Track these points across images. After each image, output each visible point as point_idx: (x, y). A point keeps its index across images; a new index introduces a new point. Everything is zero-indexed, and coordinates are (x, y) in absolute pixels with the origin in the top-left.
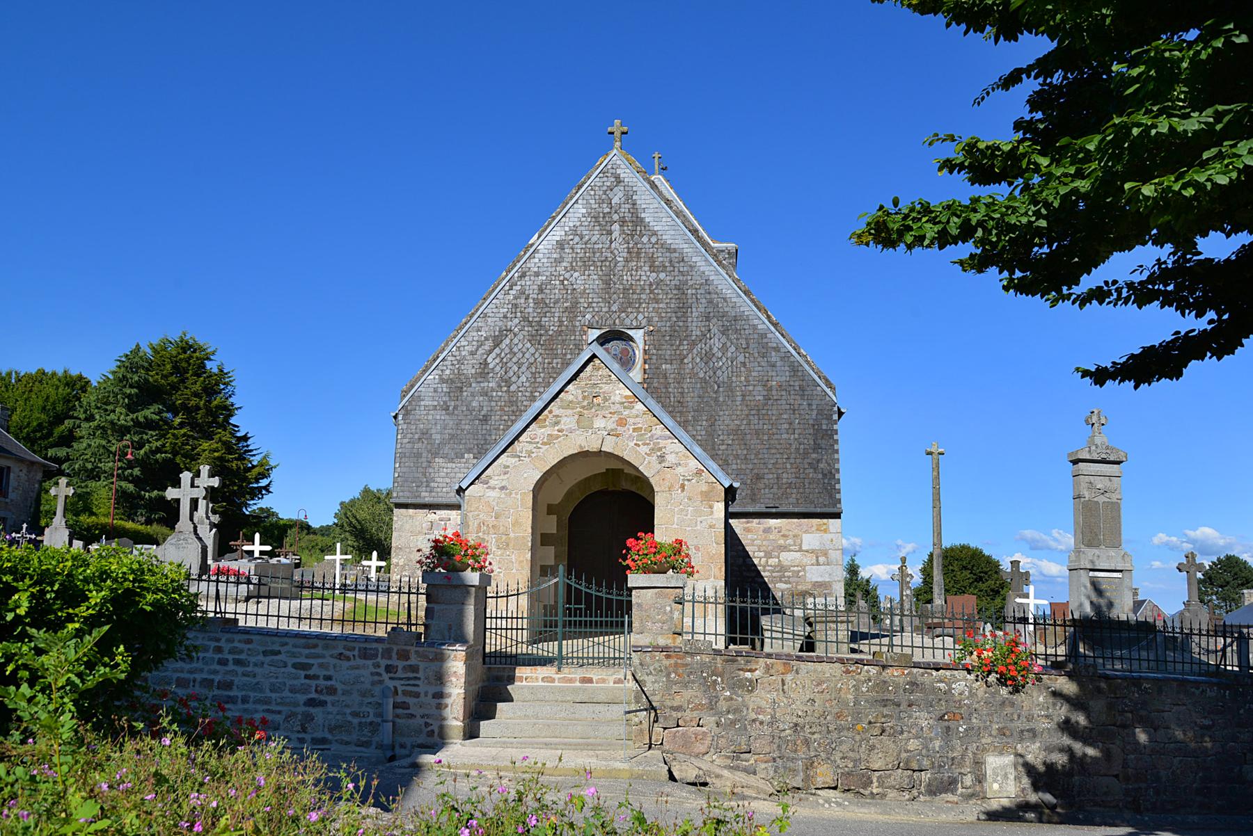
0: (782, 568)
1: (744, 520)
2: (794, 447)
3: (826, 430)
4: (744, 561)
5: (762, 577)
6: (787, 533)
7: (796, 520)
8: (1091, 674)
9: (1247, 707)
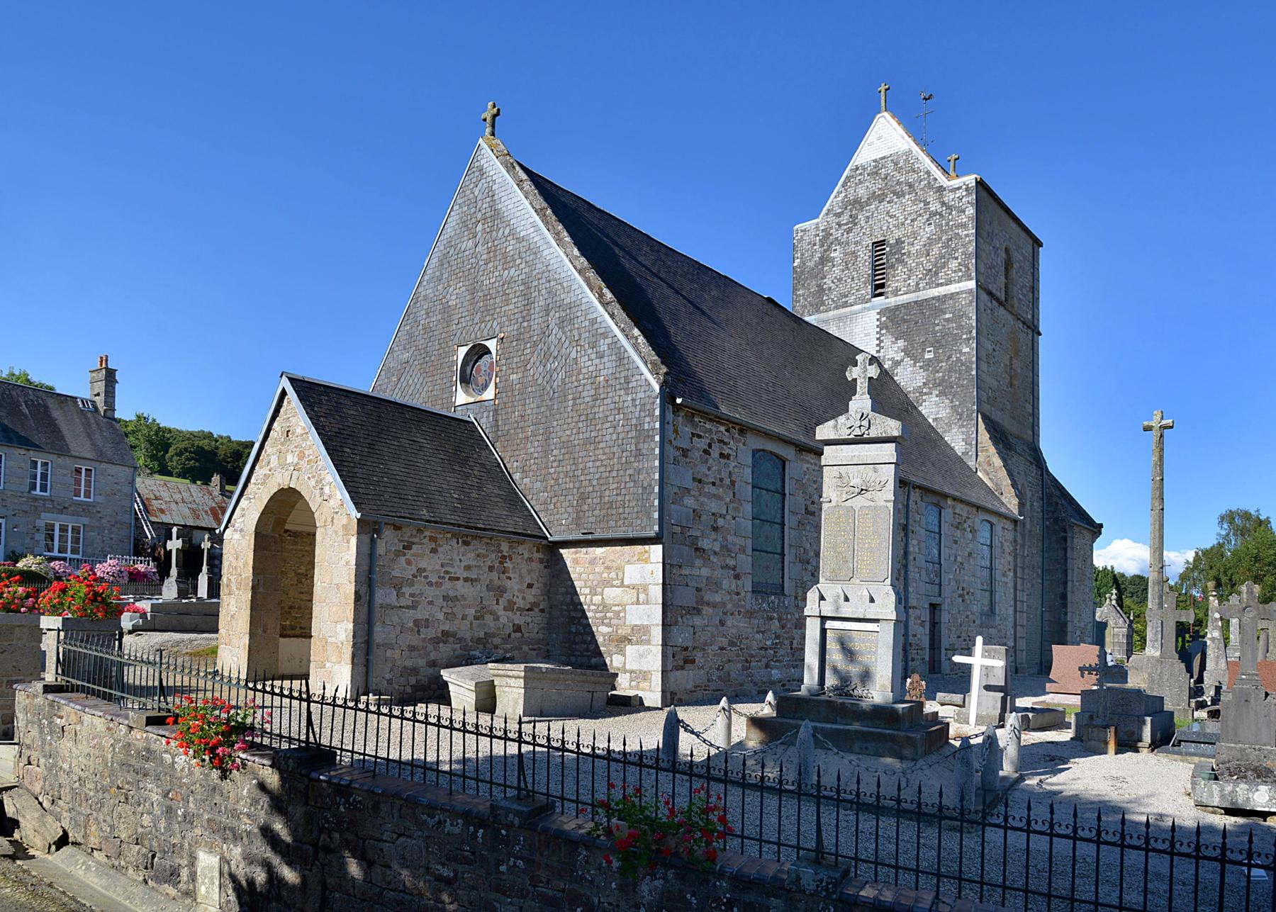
0: (604, 607)
1: (573, 550)
2: (617, 455)
3: (648, 430)
4: (572, 599)
5: (587, 618)
6: (610, 564)
7: (619, 548)
8: (290, 769)
9: (511, 863)
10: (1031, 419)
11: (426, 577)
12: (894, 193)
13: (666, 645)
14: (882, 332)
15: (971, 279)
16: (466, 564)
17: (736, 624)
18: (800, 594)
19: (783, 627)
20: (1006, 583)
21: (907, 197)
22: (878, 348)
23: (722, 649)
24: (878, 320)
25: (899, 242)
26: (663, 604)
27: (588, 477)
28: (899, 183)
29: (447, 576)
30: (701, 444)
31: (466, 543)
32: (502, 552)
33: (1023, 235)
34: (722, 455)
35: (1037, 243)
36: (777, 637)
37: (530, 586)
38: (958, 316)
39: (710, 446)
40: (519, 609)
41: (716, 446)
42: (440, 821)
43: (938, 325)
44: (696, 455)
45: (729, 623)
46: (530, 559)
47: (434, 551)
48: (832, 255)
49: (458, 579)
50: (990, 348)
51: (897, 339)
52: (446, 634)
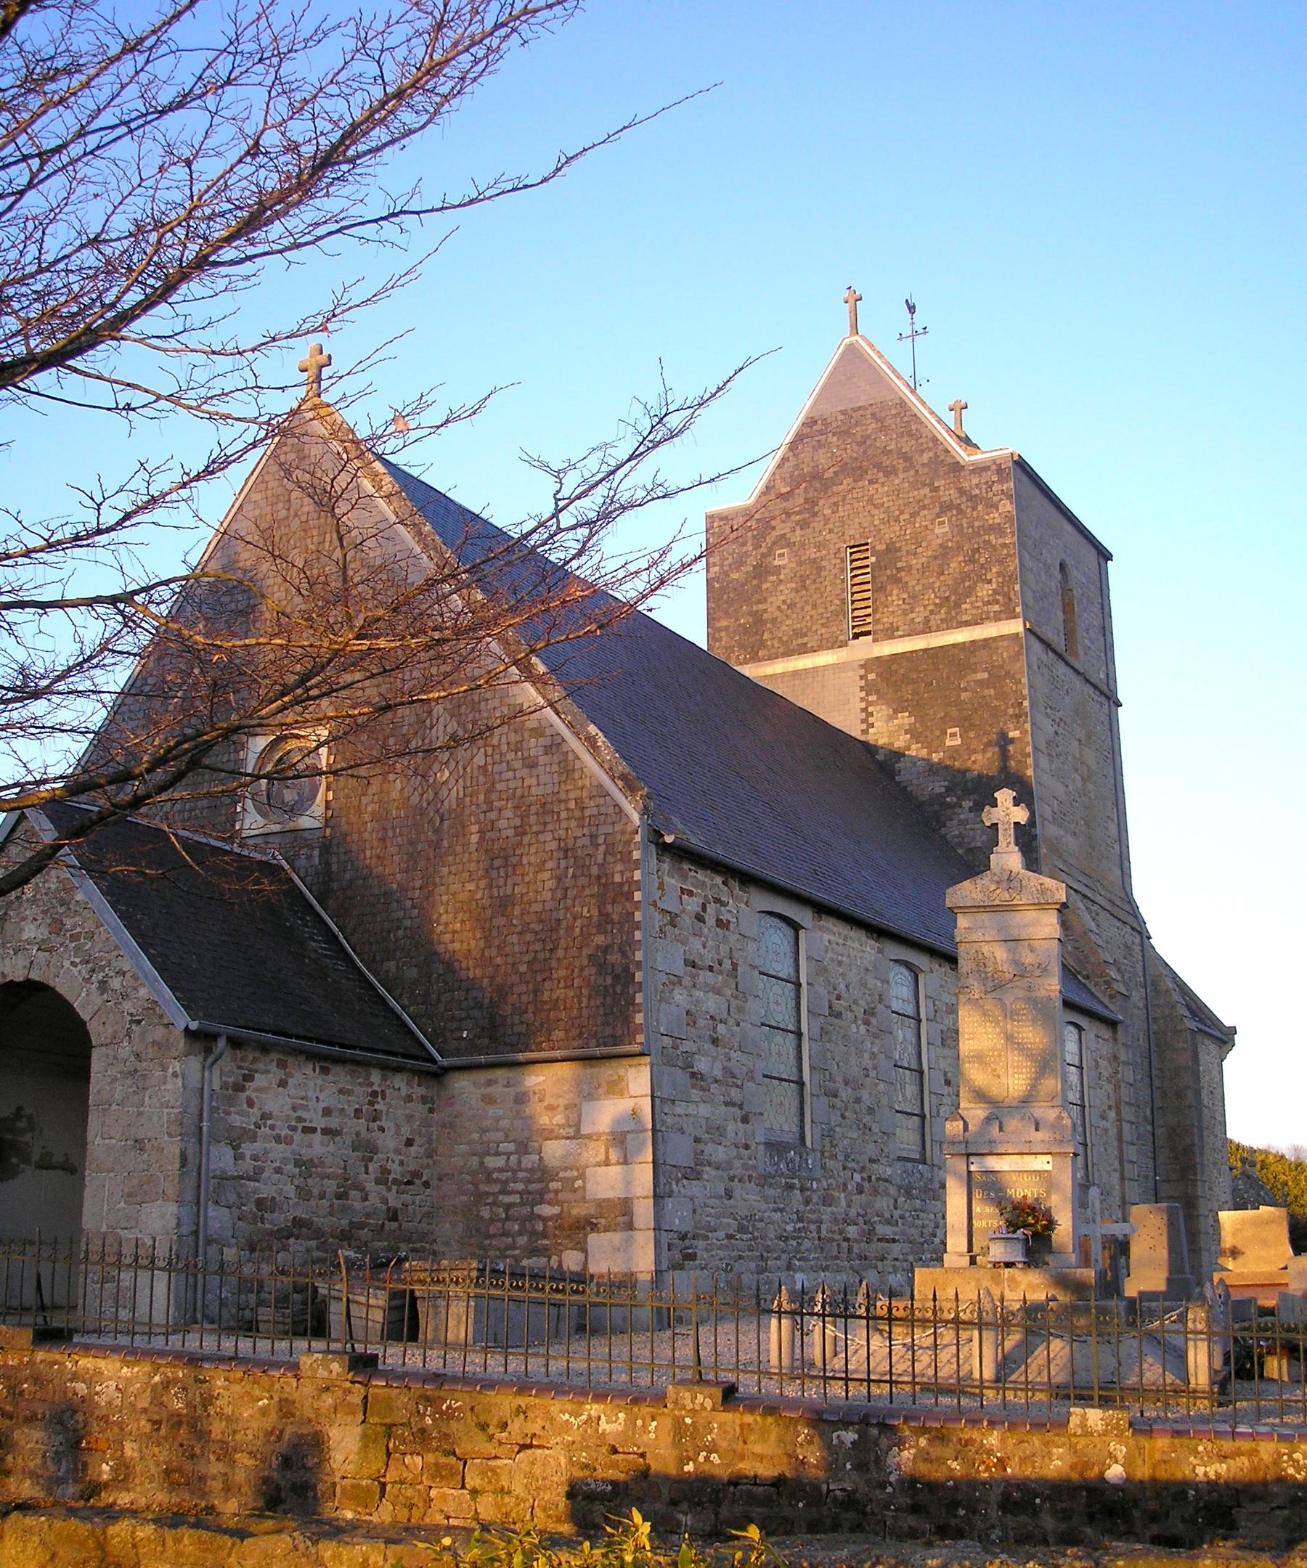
2: (564, 924)
3: (621, 884)
10: (1117, 846)
11: (272, 1128)
12: (879, 466)
13: (660, 1229)
14: (871, 698)
15: (1015, 617)
16: (325, 1105)
17: (749, 1198)
18: (827, 1148)
19: (807, 1202)
20: (1106, 1131)
21: (901, 476)
22: (864, 726)
23: (730, 1237)
24: (861, 678)
25: (891, 549)
26: (654, 1162)
27: (510, 960)
28: (885, 452)
29: (300, 1126)
30: (692, 905)
31: (325, 1071)
32: (371, 1084)
33: (1083, 541)
34: (720, 923)
35: (1105, 556)
36: (800, 1220)
37: (409, 1143)
38: (998, 676)
39: (704, 907)
40: (395, 1181)
41: (711, 908)
42: (590, 1417)
43: (966, 690)
44: (687, 921)
45: (736, 1194)
46: (409, 1098)
47: (283, 1084)
48: (776, 563)
49: (314, 1130)
50: (1051, 730)
51: (896, 711)
52: (298, 1222)
